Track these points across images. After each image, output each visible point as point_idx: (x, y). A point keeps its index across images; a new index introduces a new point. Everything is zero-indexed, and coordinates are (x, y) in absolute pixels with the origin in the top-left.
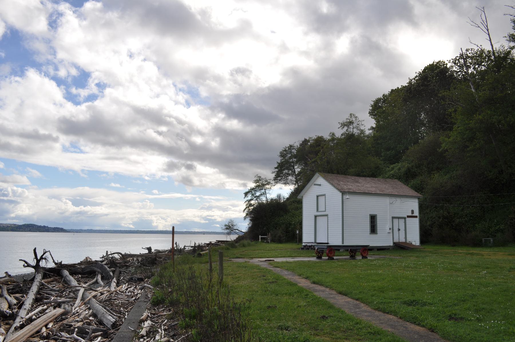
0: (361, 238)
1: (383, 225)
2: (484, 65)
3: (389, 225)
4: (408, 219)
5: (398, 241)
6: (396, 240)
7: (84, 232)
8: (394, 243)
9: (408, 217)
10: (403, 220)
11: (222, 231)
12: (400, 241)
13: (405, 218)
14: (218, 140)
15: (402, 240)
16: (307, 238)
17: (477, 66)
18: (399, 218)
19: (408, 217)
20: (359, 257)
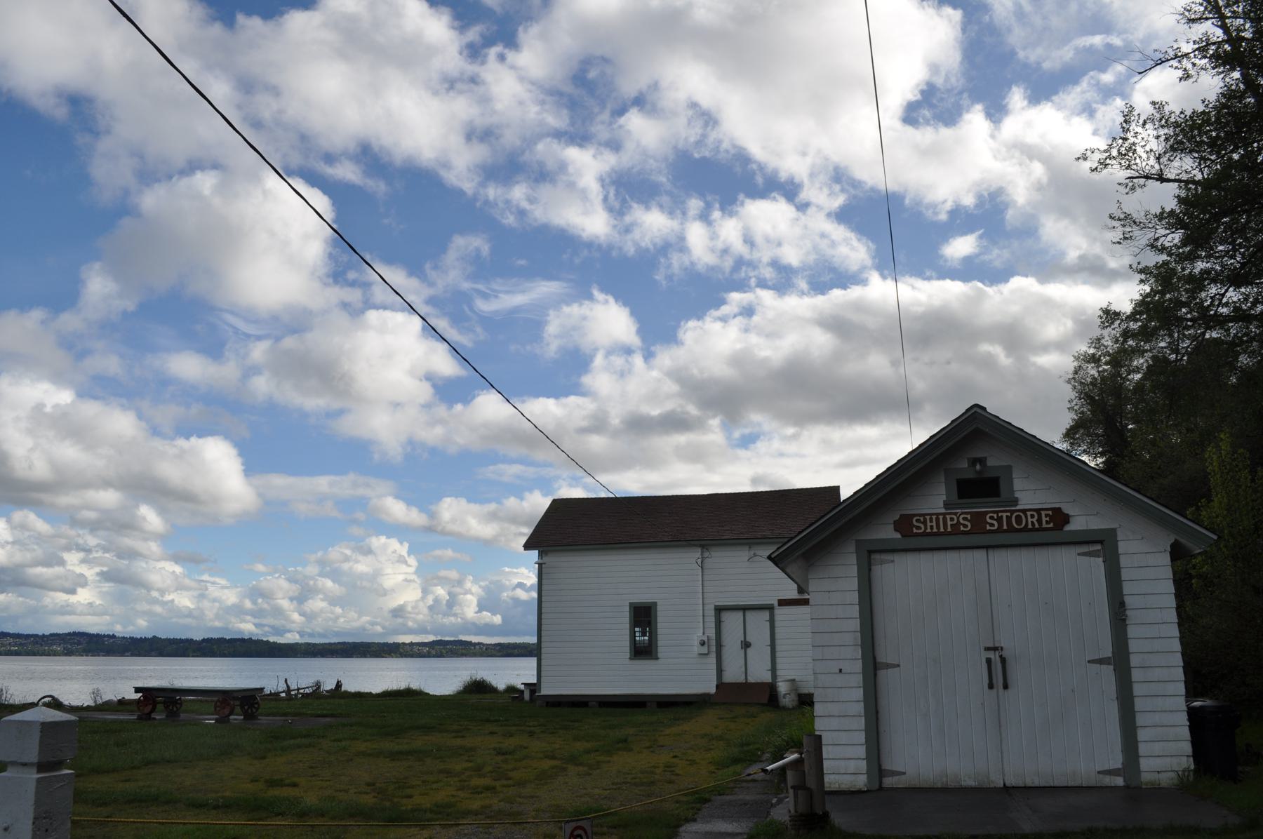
0: (609, 673)
1: (682, 635)
2: (1137, 370)
3: (701, 629)
4: (781, 612)
5: (741, 679)
6: (733, 674)
7: (474, 655)
8: (721, 686)
9: (783, 603)
10: (766, 615)
11: (714, 655)
12: (751, 680)
13: (770, 608)
14: (1098, 244)
15: (759, 673)
16: (534, 681)
17: (1173, 357)
18: (744, 609)
19: (783, 603)
20: (237, 718)
